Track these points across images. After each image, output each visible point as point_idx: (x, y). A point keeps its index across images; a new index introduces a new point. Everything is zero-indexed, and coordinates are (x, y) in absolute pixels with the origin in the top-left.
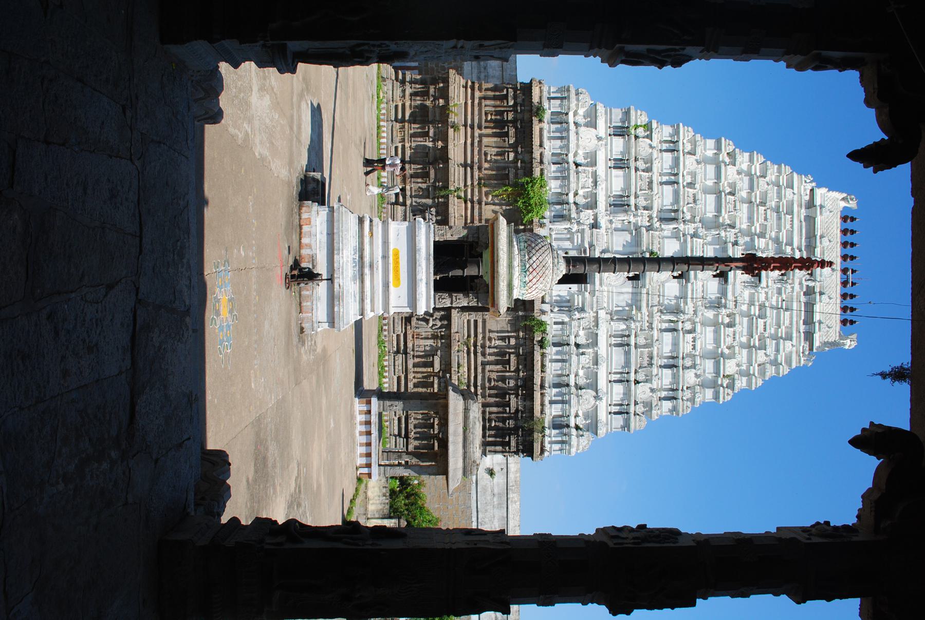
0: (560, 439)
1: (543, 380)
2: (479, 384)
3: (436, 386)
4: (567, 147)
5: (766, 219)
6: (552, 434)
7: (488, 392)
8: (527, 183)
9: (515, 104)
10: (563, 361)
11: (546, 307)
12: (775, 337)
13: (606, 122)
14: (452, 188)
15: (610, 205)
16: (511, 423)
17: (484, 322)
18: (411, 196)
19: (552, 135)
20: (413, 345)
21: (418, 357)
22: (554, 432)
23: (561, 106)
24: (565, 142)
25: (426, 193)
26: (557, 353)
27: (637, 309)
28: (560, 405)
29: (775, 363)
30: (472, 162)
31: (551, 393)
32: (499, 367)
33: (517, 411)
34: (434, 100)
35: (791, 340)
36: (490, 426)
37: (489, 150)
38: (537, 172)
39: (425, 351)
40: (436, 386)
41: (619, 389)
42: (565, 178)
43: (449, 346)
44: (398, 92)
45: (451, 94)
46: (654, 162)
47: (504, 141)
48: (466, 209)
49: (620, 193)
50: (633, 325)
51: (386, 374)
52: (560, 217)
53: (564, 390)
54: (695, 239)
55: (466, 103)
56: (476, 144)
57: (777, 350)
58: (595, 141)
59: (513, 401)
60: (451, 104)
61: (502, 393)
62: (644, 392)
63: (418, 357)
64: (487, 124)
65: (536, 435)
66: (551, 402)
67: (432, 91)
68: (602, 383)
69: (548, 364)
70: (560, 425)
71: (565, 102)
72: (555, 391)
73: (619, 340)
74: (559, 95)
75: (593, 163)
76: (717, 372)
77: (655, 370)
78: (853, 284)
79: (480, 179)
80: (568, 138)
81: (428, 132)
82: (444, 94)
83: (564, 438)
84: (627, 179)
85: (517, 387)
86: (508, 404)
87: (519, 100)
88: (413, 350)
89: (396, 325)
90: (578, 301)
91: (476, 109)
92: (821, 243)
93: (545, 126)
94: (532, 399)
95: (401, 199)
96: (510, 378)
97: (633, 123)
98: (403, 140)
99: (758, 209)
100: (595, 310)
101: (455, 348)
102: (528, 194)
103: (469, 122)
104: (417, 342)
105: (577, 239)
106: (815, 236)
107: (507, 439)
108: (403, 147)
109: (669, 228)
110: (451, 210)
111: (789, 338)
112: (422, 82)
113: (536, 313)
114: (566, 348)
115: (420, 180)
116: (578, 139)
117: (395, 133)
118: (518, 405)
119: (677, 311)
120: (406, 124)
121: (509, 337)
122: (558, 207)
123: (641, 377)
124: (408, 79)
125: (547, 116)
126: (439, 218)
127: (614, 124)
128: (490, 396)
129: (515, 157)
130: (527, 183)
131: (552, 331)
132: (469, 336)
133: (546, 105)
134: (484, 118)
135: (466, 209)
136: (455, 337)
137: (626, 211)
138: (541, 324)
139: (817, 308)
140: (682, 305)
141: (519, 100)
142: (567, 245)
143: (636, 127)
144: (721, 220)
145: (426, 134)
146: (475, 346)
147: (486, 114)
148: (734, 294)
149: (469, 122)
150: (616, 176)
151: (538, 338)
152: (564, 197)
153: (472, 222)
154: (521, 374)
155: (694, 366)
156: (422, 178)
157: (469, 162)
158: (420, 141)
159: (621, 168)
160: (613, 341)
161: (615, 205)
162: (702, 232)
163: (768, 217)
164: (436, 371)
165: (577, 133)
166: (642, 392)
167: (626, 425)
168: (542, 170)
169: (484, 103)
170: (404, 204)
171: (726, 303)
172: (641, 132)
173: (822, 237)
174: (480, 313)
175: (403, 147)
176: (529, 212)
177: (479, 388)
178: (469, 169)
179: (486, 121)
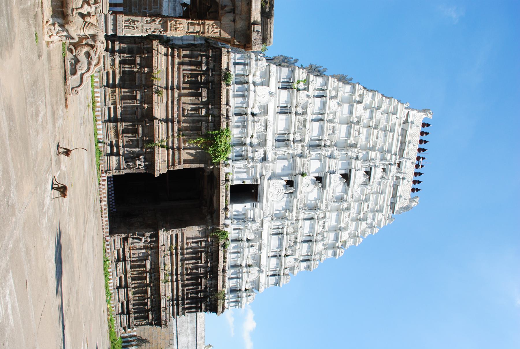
0: (235, 300)
1: (224, 267)
2: (179, 273)
3: (148, 279)
4: (247, 103)
5: (377, 138)
6: (230, 297)
7: (185, 277)
8: (216, 135)
9: (208, 69)
10: (238, 252)
11: (228, 222)
12: (374, 211)
13: (276, 79)
14: (156, 142)
15: (276, 140)
16: (202, 295)
17: (183, 234)
18: (123, 147)
19: (236, 93)
20: (130, 254)
21: (134, 261)
22: (231, 296)
23: (243, 70)
24: (246, 99)
25: (135, 143)
26: (234, 247)
27: (289, 211)
28: (235, 280)
29: (371, 227)
30: (173, 116)
31: (230, 272)
32: (194, 261)
33: (206, 287)
34: (140, 68)
35: (382, 212)
36: (187, 297)
37: (186, 106)
38: (224, 126)
39: (139, 257)
40: (148, 279)
41: (274, 261)
42: (245, 127)
43: (157, 253)
44: (109, 61)
45: (155, 64)
46: (309, 106)
47: (199, 99)
48: (168, 154)
49: (283, 132)
50: (286, 223)
51: (111, 277)
52: (240, 157)
53: (237, 270)
54: (331, 160)
55: (167, 69)
56: (176, 103)
57: (374, 219)
58: (268, 96)
59: (204, 282)
60: (155, 72)
61: (196, 277)
62: (290, 261)
63: (134, 261)
64: (185, 85)
65: (219, 302)
66: (229, 279)
67: (138, 60)
68: (263, 261)
69: (228, 256)
70: (233, 291)
71: (248, 67)
72: (232, 271)
73: (275, 231)
74: (242, 61)
75: (266, 113)
76: (336, 240)
77: (300, 223)
78: (422, 166)
79: (179, 130)
80: (248, 97)
81: (136, 96)
82: (149, 63)
83: (238, 299)
84: (289, 123)
85: (206, 273)
86: (200, 284)
87: (211, 65)
88: (130, 257)
89: (116, 244)
90: (250, 214)
91: (176, 73)
92: (408, 146)
93: (231, 88)
94: (217, 279)
95: (115, 150)
96: (201, 267)
97: (296, 80)
98: (114, 103)
99: (373, 132)
100: (262, 218)
101: (161, 256)
102: (217, 144)
103: (170, 84)
104: (132, 252)
105: (252, 172)
106: (405, 142)
107: (199, 305)
108: (115, 109)
109: (314, 154)
110: (156, 158)
111: (381, 210)
112: (130, 51)
113: (221, 227)
114: (241, 244)
115: (130, 135)
116: (255, 96)
117: (107, 97)
118: (207, 283)
119: (315, 208)
120: (117, 89)
121: (201, 242)
122: (238, 148)
123: (289, 252)
124: (117, 49)
125: (232, 80)
126: (147, 164)
127: (282, 80)
128: (187, 279)
129: (207, 112)
130: (216, 135)
131: (232, 234)
132: (172, 244)
133: (232, 69)
134: (182, 79)
135: (168, 154)
136: (161, 248)
137: (287, 146)
138: (225, 233)
139: (400, 188)
140: (319, 204)
141: (211, 65)
142: (244, 176)
143: (299, 82)
144: (349, 142)
145: (134, 98)
146: (176, 249)
147: (184, 76)
148: (352, 192)
149: (170, 84)
150: (282, 120)
151: (221, 242)
152: (243, 139)
153: (173, 164)
154: (209, 264)
155: (322, 240)
156: (132, 133)
157: (170, 117)
158: (129, 103)
159: (285, 113)
160: (272, 231)
161: (279, 141)
162: (336, 153)
163: (379, 136)
164: (148, 270)
165: (255, 91)
166: (289, 262)
167: (278, 283)
168: (227, 123)
169: (182, 67)
170: (118, 154)
171: (346, 198)
172: (301, 86)
173: (409, 143)
174: (180, 229)
175: (115, 109)
176: (217, 157)
177: (179, 276)
178: (170, 124)
179: (184, 83)
